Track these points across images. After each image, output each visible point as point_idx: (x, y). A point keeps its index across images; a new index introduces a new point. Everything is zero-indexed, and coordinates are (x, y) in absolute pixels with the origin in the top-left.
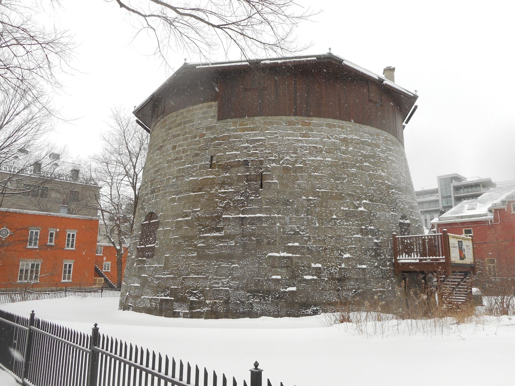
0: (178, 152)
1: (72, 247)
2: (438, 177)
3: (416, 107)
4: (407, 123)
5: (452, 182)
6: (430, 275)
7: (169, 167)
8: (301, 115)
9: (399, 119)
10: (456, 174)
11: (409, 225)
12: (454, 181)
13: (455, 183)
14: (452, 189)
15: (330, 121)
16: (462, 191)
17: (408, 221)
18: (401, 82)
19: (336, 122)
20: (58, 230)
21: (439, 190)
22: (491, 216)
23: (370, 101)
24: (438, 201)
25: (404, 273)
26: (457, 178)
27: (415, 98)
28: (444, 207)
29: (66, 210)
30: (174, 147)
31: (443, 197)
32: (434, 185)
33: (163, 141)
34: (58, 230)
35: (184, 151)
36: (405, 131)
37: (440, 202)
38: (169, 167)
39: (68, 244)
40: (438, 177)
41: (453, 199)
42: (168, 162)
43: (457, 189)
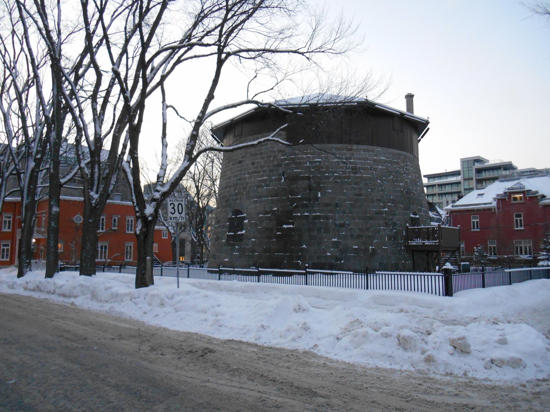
0: (257, 167)
1: (102, 229)
2: (461, 159)
3: (428, 129)
4: (422, 137)
5: (474, 165)
6: (93, 205)
7: (250, 178)
8: (346, 143)
9: (415, 136)
10: (479, 157)
11: (418, 218)
12: (476, 164)
13: (478, 165)
14: (474, 171)
15: (365, 147)
16: (483, 174)
17: (418, 216)
18: (419, 113)
19: (370, 148)
20: (120, 216)
21: (462, 172)
22: (494, 204)
23: (393, 130)
24: (460, 183)
25: (413, 251)
26: (478, 160)
27: (427, 123)
28: (465, 190)
29: (120, 197)
30: (253, 164)
31: (465, 180)
32: (457, 167)
33: (243, 157)
34: (120, 216)
35: (262, 167)
36: (420, 144)
37: (462, 184)
38: (250, 178)
39: (128, 230)
40: (461, 159)
41: (474, 181)
42: (249, 173)
43: (479, 171)
